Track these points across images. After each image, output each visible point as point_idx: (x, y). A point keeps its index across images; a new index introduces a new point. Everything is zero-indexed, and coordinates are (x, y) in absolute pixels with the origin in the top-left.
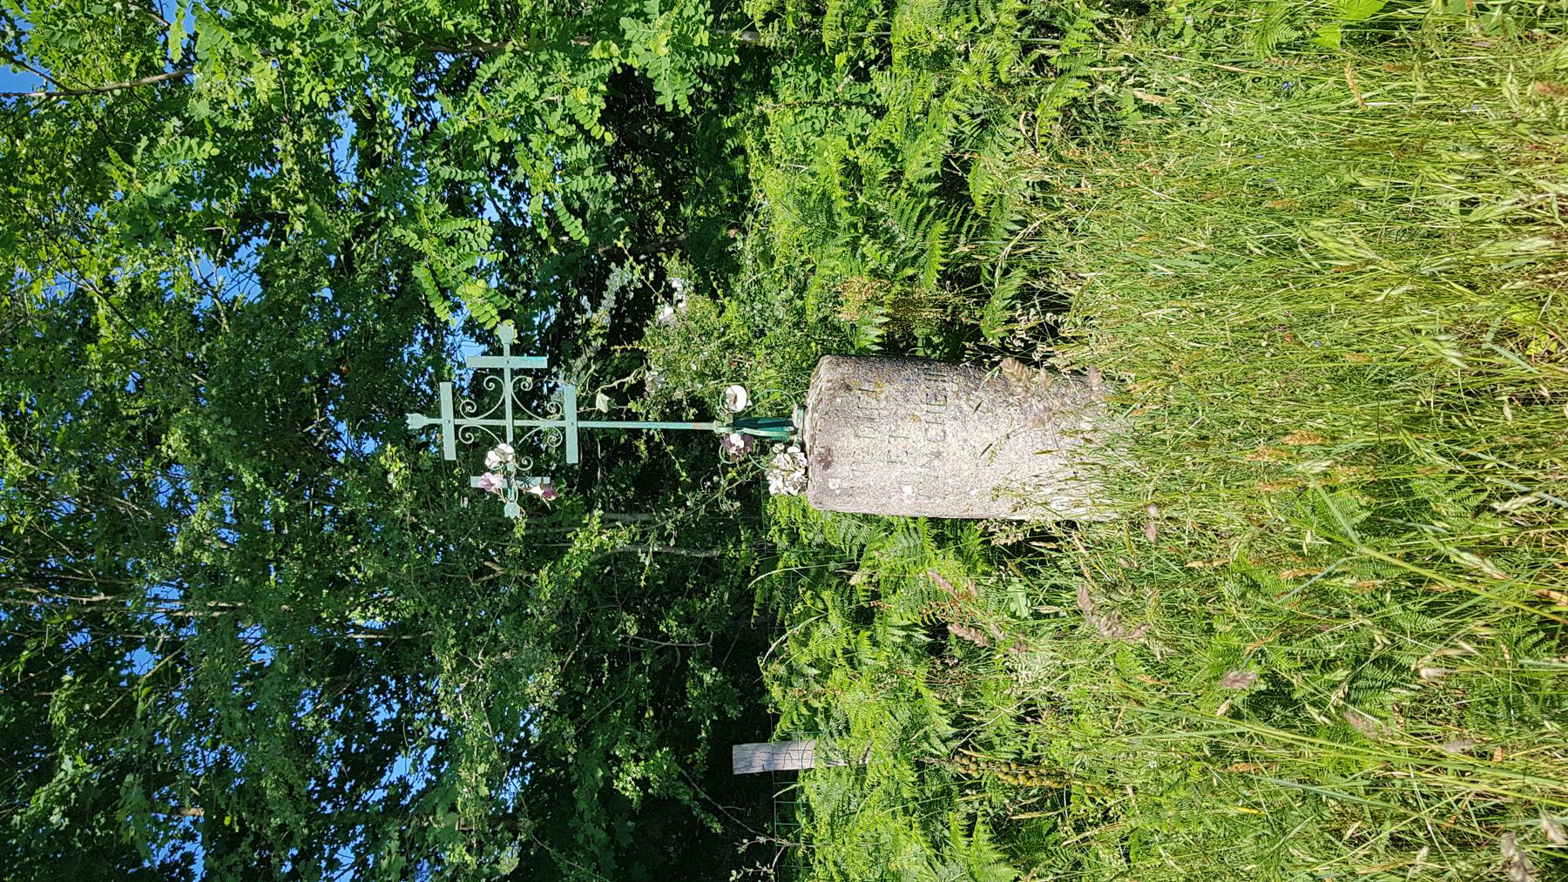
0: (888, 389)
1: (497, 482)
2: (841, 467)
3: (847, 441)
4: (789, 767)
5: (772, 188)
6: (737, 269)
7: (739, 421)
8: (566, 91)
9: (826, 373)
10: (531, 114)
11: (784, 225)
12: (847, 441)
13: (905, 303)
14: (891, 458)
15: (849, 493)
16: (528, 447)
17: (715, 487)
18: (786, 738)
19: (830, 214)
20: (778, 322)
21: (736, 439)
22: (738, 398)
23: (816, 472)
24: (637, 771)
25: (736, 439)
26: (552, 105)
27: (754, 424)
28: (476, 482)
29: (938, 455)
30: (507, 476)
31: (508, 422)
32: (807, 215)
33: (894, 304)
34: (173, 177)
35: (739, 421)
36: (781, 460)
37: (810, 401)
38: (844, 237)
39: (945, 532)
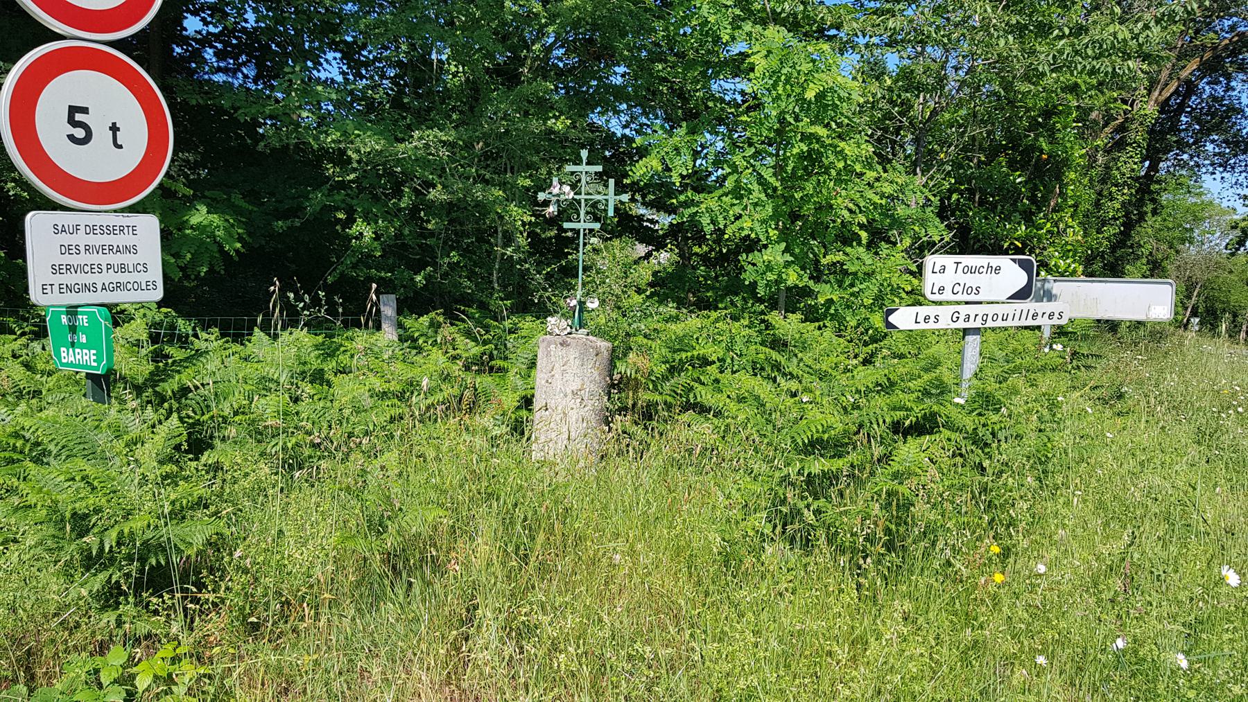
0: (596, 373)
1: (556, 191)
2: (561, 352)
3: (572, 354)
4: (384, 326)
5: (693, 322)
6: (660, 302)
7: (581, 303)
8: (750, 216)
9: (604, 345)
10: (741, 197)
11: (677, 328)
12: (572, 354)
13: (637, 386)
14: (563, 369)
15: (548, 354)
16: (574, 205)
17: (545, 290)
18: (400, 325)
19: (680, 350)
20: (630, 325)
21: (574, 303)
22: (593, 304)
23: (559, 340)
24: (368, 233)
25: (574, 303)
26: (745, 208)
27: (581, 311)
28: (555, 180)
29: (566, 396)
30: (558, 195)
31: (583, 197)
32: (680, 340)
33: (636, 379)
34: (712, 19)
35: (581, 303)
36: (564, 323)
37: (590, 337)
38: (669, 355)
39: (527, 402)
